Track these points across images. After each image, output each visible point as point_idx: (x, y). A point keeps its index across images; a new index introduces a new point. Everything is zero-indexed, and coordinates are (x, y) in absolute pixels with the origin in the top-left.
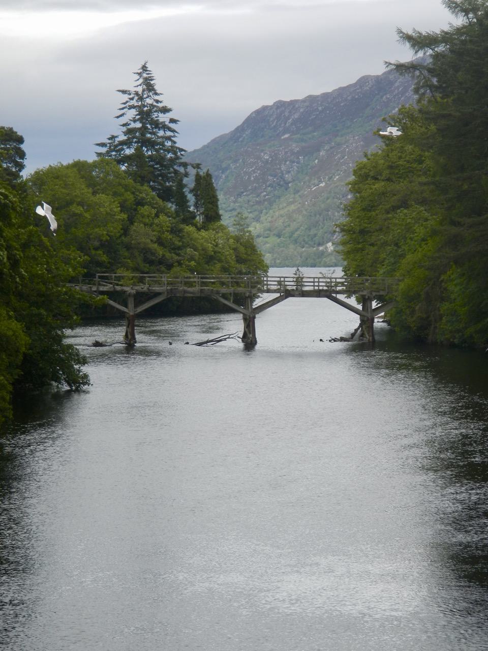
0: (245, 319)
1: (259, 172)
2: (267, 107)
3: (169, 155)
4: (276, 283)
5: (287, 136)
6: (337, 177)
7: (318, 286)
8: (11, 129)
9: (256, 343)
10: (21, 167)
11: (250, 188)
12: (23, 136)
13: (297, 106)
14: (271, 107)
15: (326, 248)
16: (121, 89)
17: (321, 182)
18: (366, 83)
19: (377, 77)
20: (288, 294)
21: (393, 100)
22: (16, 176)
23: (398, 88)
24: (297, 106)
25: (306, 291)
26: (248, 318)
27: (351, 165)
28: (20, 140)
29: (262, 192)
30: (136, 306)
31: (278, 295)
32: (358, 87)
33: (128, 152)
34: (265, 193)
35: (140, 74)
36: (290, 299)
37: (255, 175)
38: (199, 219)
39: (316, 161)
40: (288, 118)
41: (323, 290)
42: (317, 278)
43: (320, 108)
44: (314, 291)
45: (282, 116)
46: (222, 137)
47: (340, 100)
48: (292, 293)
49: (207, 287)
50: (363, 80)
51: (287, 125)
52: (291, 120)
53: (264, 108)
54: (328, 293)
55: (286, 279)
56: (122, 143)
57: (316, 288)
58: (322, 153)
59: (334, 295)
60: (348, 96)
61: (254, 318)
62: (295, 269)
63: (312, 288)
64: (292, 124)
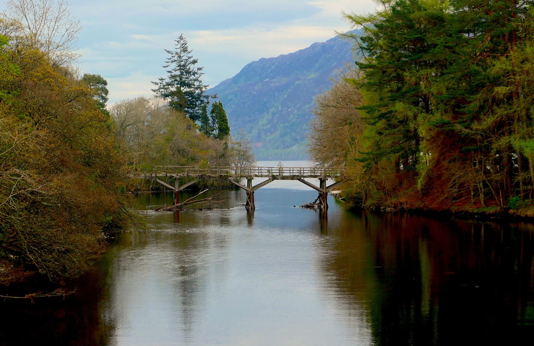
2: (255, 62)
3: (197, 91)
4: (266, 171)
5: (267, 80)
7: (293, 173)
8: (99, 76)
10: (106, 100)
14: (258, 62)
19: (323, 43)
22: (103, 105)
25: (285, 176)
28: (105, 83)
30: (179, 186)
31: (268, 178)
33: (173, 89)
35: (178, 42)
38: (216, 132)
44: (291, 176)
46: (227, 80)
48: (277, 177)
55: (305, 169)
56: (168, 84)
57: (291, 174)
62: (279, 162)
63: (288, 174)
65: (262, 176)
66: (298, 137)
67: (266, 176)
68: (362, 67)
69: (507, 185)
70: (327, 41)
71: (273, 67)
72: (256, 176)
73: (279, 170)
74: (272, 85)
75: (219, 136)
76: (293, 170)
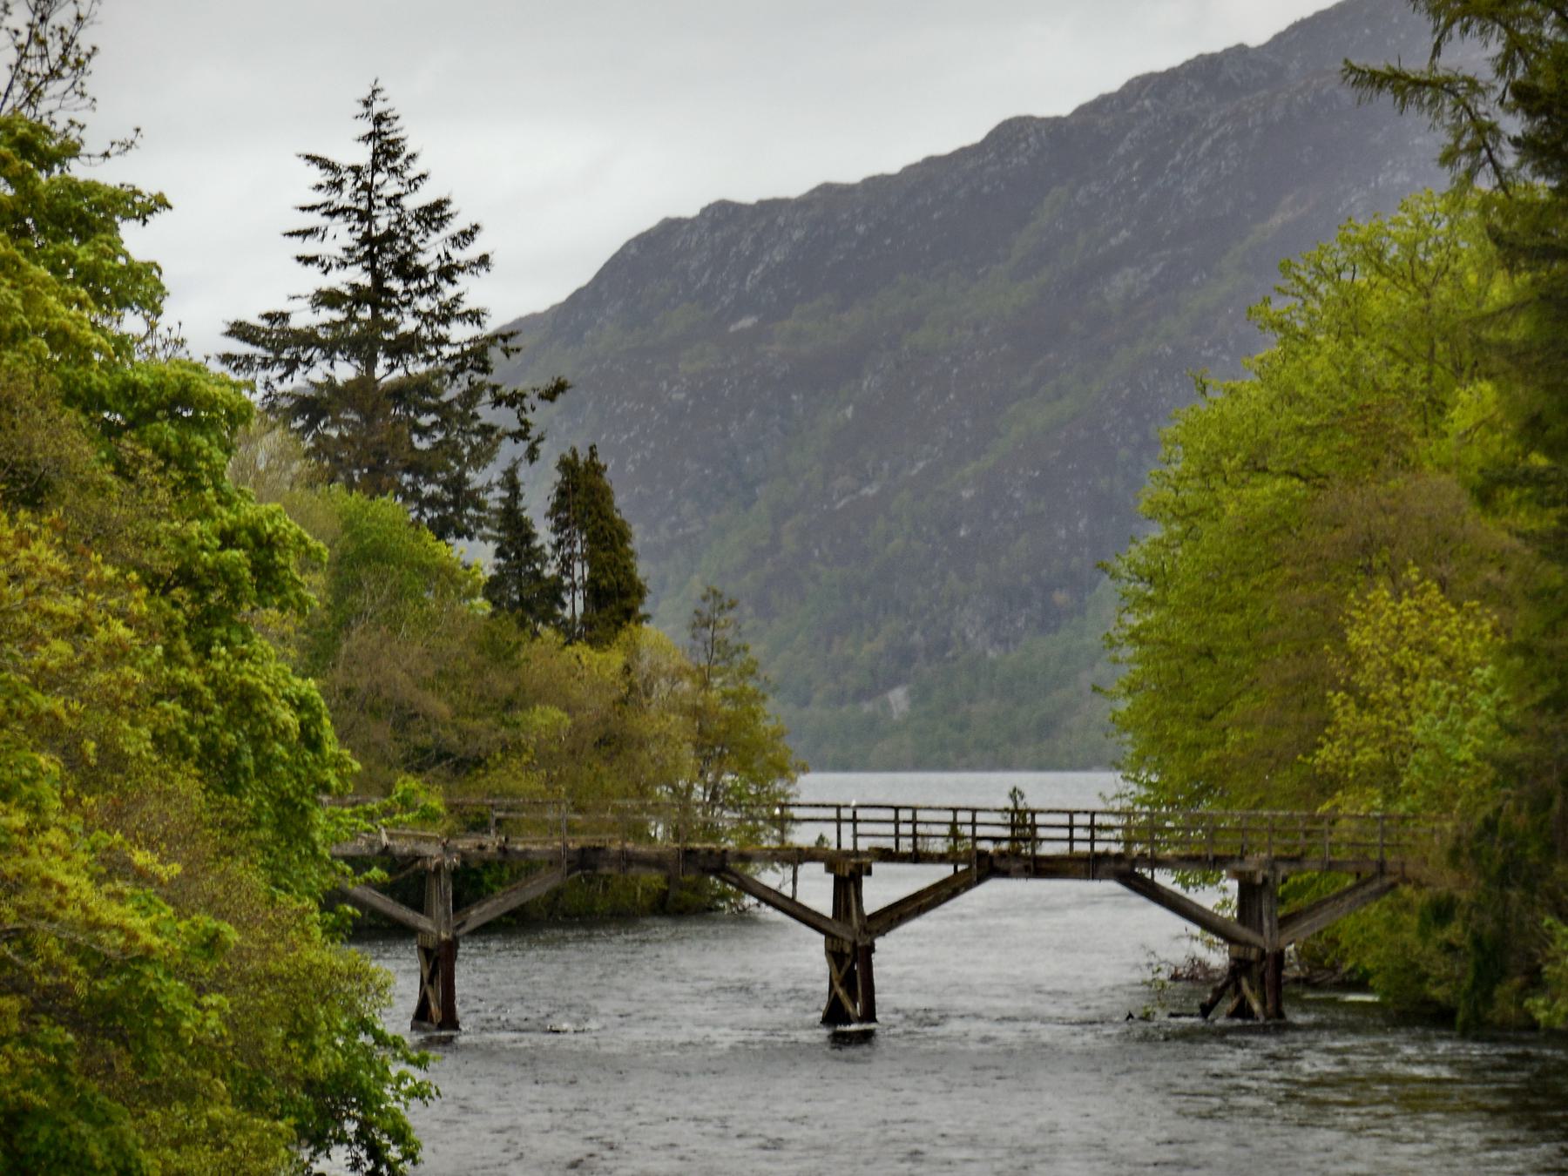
1: (652, 445)
5: (747, 322)
6: (921, 465)
7: (1092, 840)
12: (242, 318)
13: (781, 220)
14: (692, 222)
15: (886, 705)
16: (314, 153)
17: (866, 480)
19: (1056, 123)
20: (985, 867)
26: (848, 949)
27: (967, 423)
31: (946, 871)
34: (673, 518)
36: (994, 889)
38: (575, 606)
39: (849, 412)
41: (1106, 856)
42: (967, 809)
48: (1001, 864)
52: (761, 267)
53: (670, 227)
58: (868, 382)
61: (871, 949)
63: (1061, 849)
65: (917, 857)
66: (917, 637)
67: (941, 859)
70: (1082, 110)
72: (887, 856)
73: (1013, 826)
75: (588, 624)
76: (914, 822)
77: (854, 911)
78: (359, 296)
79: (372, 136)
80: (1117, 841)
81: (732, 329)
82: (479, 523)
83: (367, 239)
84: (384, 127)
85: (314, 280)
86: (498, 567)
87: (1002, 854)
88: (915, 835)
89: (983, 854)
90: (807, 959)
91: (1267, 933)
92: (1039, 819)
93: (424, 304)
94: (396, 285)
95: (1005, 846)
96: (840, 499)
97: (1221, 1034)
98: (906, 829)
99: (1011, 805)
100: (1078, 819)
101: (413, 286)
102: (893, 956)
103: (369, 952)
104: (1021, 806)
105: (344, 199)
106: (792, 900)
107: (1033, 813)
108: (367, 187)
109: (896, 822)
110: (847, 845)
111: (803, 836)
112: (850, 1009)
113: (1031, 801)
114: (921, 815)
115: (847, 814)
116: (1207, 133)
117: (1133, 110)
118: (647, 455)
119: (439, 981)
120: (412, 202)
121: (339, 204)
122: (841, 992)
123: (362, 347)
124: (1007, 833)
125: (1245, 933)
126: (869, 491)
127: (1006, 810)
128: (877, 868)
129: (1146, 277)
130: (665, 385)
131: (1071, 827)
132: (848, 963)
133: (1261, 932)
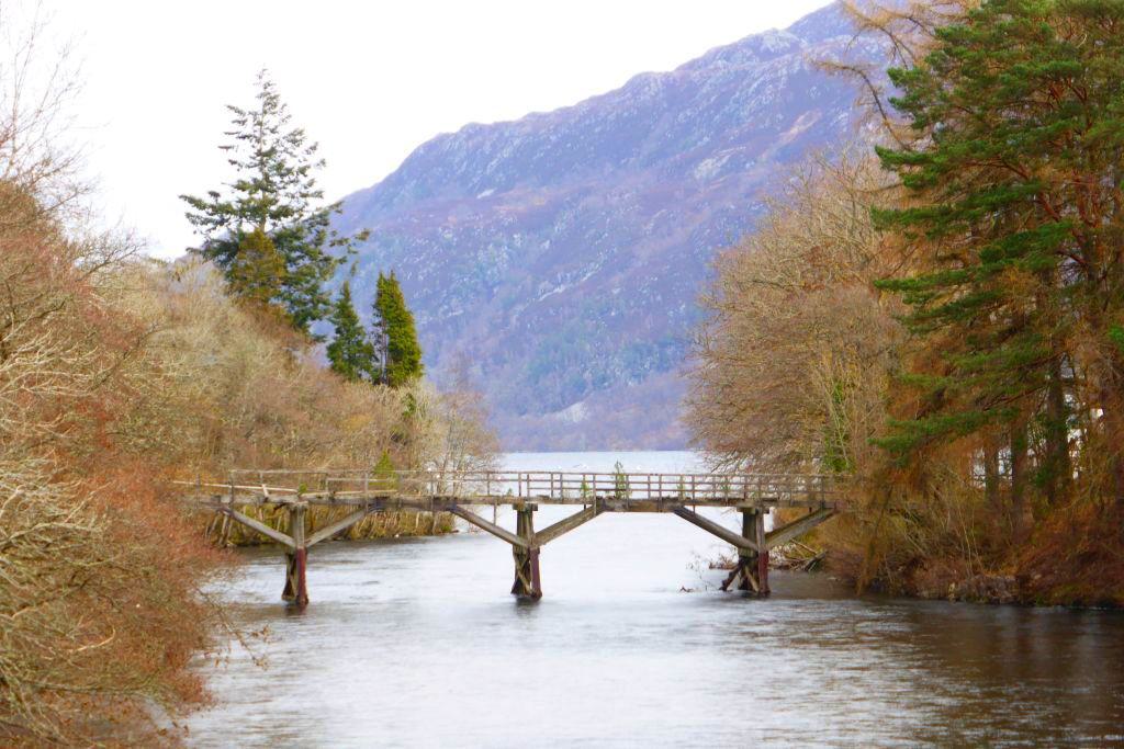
0: (518, 555)
2: (447, 136)
5: (488, 193)
7: (660, 490)
9: (540, 595)
11: (416, 295)
13: (507, 134)
14: (456, 136)
18: (644, 87)
19: (667, 75)
20: (600, 506)
21: (698, 120)
23: (707, 96)
24: (507, 134)
25: (636, 501)
26: (525, 552)
29: (440, 305)
32: (629, 95)
34: (446, 307)
36: (606, 515)
37: (425, 271)
40: (491, 157)
43: (553, 138)
45: (478, 153)
47: (593, 121)
48: (611, 504)
49: (246, 468)
50: (638, 85)
51: (488, 171)
54: (679, 506)
55: (598, 478)
57: (655, 495)
59: (690, 508)
60: (609, 113)
63: (643, 495)
64: (497, 171)
65: (563, 501)
66: (587, 375)
67: (577, 501)
68: (888, 160)
69: (226, 530)
71: (506, 153)
72: (546, 499)
73: (617, 483)
74: (502, 210)
76: (561, 481)
77: (528, 531)
78: (258, 186)
79: (262, 96)
80: (675, 491)
81: (479, 197)
82: (326, 312)
83: (259, 153)
84: (268, 90)
85: (236, 175)
86: (335, 338)
87: (610, 498)
88: (561, 488)
89: (599, 499)
90: (500, 563)
91: (759, 542)
92: (631, 479)
93: (291, 189)
94: (277, 179)
95: (612, 494)
96: (543, 294)
97: (732, 599)
98: (557, 485)
99: (616, 471)
100: (653, 479)
101: (286, 179)
102: (550, 558)
103: (319, 556)
104: (621, 472)
105: (248, 129)
106: (494, 525)
107: (628, 476)
108: (260, 124)
109: (552, 481)
110: (524, 494)
111: (503, 490)
112: (527, 593)
113: (627, 469)
114: (565, 477)
115: (524, 477)
116: (755, 80)
117: (712, 67)
118: (431, 270)
119: (296, 576)
120: (285, 130)
121: (245, 132)
122: (521, 576)
123: (257, 211)
124: (613, 486)
125: (747, 542)
126: (559, 290)
127: (613, 474)
128: (542, 507)
129: (719, 165)
130: (440, 229)
131: (649, 483)
132: (525, 560)
133: (756, 542)
